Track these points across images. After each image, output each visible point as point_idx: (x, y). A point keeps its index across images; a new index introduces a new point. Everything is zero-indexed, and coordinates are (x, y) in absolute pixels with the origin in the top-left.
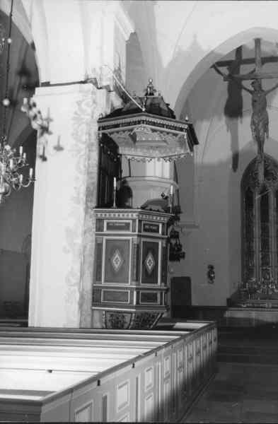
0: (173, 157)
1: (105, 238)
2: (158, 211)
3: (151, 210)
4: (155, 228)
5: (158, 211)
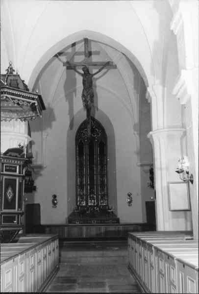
0: (27, 119)
1: (5, 177)
2: (16, 156)
3: (10, 156)
4: (13, 169)
5: (16, 156)
